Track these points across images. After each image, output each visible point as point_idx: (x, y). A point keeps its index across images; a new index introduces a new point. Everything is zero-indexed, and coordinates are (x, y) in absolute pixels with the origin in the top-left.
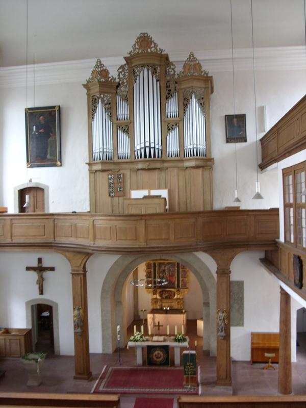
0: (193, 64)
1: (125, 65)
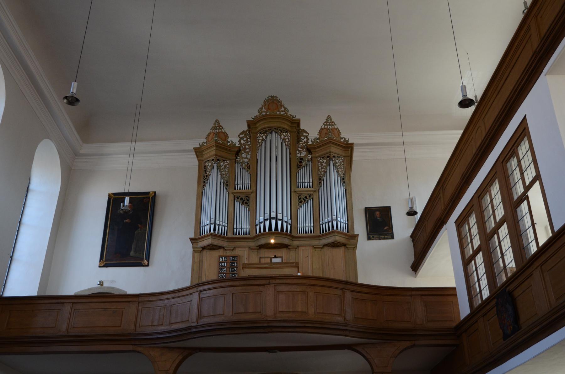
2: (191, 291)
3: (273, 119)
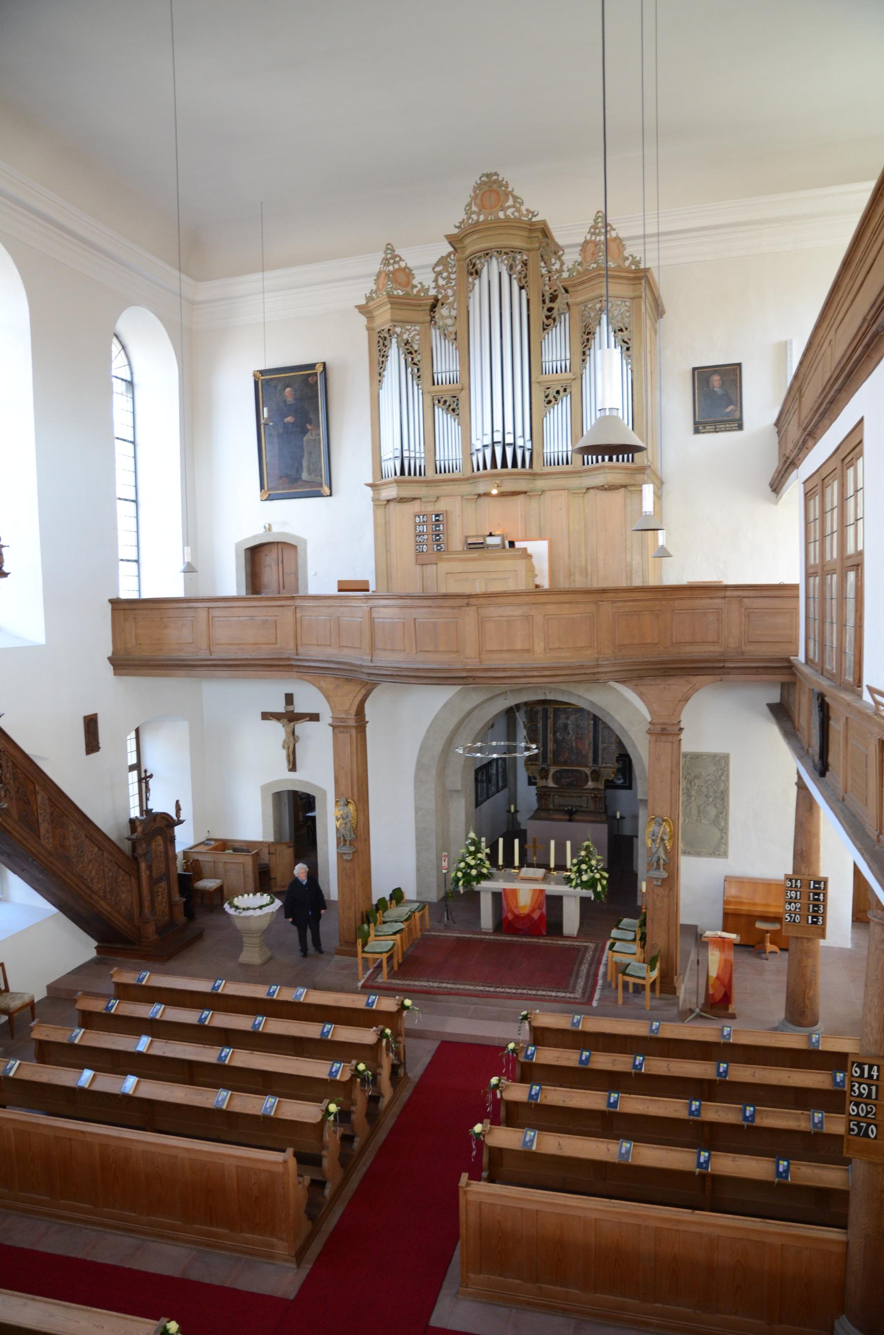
0: (603, 239)
1: (449, 255)
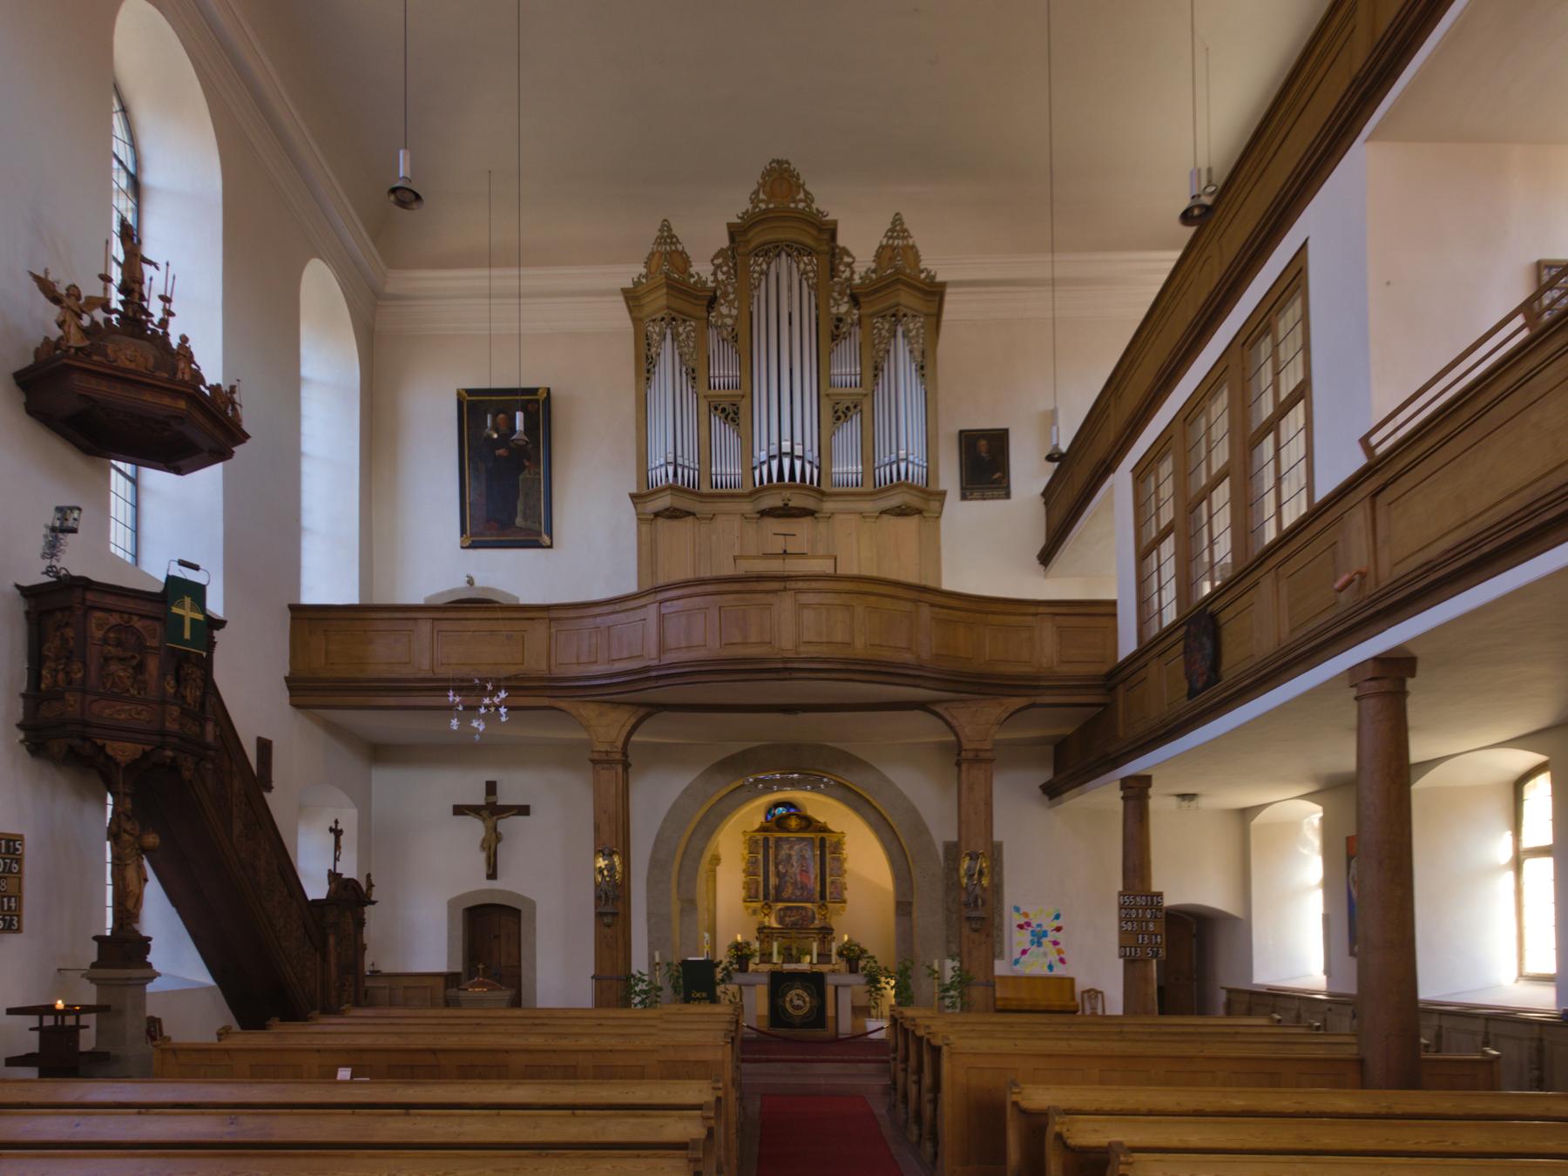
0: (897, 253)
2: (643, 601)
3: (783, 226)
